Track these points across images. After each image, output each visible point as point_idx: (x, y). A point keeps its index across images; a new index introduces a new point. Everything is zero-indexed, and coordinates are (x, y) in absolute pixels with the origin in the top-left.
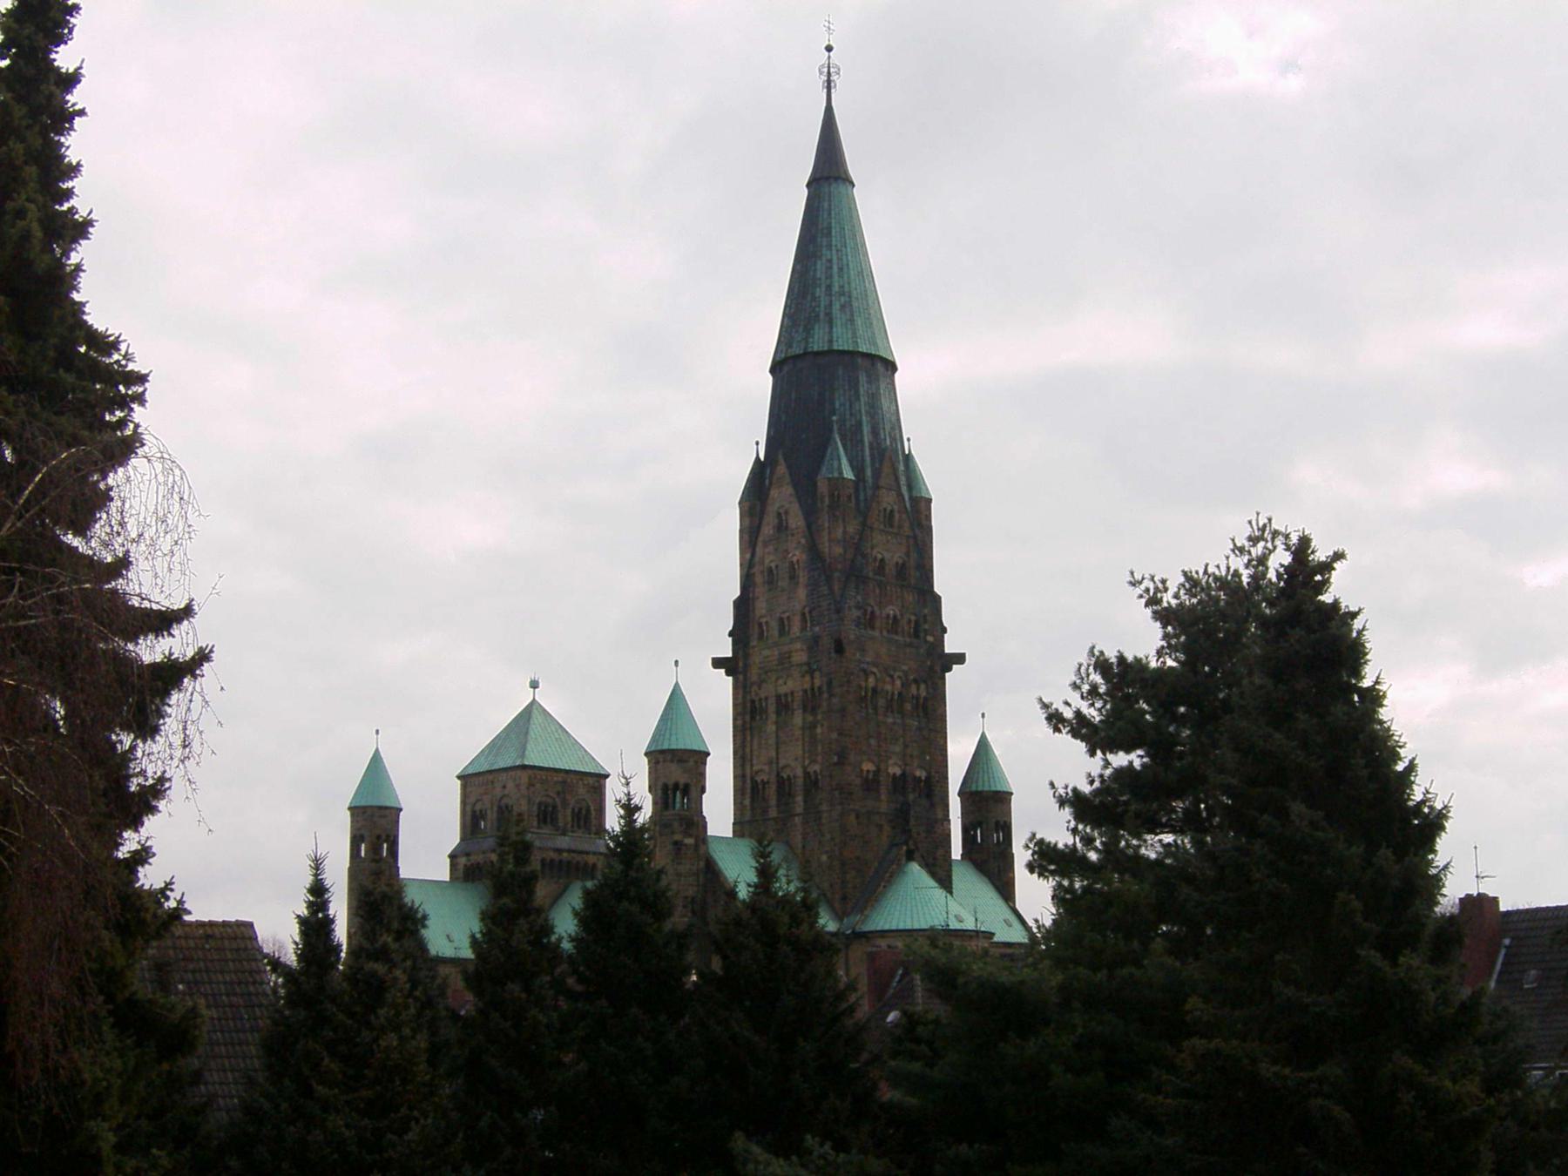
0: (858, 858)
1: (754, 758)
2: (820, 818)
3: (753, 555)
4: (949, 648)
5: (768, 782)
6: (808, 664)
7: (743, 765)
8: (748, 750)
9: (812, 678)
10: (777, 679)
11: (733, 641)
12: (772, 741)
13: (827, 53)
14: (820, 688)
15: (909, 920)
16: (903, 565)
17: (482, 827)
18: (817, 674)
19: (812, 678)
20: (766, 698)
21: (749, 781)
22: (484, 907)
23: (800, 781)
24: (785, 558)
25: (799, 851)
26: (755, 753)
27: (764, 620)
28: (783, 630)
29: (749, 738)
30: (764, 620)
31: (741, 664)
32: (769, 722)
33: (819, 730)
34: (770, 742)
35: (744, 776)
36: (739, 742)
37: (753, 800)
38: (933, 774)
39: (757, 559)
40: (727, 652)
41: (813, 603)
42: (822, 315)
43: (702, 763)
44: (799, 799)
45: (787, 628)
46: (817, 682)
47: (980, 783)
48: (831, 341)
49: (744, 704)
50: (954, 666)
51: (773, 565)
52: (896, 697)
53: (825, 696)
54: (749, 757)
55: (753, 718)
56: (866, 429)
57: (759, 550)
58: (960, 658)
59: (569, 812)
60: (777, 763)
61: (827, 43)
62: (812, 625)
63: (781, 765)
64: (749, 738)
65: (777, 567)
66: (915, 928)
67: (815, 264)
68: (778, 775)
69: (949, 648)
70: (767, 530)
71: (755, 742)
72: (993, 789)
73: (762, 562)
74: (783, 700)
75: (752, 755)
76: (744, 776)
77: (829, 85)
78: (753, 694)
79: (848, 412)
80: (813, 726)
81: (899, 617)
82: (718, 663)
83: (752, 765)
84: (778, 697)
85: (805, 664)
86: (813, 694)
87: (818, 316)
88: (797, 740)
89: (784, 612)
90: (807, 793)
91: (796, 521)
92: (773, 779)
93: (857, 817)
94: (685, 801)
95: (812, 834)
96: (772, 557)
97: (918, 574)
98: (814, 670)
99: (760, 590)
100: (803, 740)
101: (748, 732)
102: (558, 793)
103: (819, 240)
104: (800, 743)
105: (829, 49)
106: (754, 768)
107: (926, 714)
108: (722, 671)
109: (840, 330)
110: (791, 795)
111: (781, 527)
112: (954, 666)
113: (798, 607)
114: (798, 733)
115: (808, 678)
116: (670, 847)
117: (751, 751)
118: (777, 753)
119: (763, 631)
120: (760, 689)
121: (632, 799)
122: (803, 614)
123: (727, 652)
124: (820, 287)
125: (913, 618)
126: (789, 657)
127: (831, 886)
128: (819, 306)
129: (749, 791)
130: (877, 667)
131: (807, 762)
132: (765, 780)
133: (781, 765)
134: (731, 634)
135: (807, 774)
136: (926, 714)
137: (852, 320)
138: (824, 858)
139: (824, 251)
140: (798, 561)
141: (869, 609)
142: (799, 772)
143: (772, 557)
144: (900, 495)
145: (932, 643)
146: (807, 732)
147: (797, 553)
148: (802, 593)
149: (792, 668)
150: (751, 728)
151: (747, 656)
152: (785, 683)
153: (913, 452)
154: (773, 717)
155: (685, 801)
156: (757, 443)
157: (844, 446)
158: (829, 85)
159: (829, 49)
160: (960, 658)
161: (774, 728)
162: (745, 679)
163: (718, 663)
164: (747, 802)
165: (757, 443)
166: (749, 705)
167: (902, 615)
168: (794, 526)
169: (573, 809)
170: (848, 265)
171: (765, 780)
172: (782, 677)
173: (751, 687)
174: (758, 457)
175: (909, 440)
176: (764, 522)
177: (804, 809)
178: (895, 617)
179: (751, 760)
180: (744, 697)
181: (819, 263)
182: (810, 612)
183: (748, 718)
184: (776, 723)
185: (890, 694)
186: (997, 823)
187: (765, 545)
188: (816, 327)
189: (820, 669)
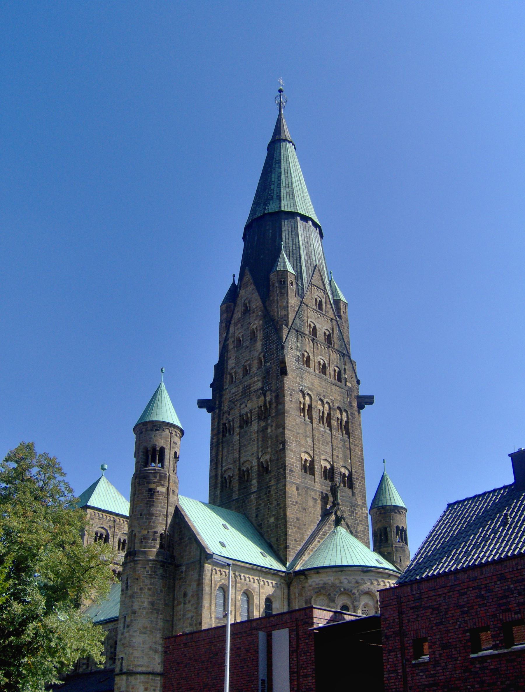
0: (298, 519)
1: (224, 461)
2: (269, 492)
3: (228, 333)
5: (232, 477)
6: (262, 388)
7: (216, 468)
8: (220, 458)
9: (265, 397)
10: (241, 405)
11: (213, 390)
12: (237, 447)
14: (270, 402)
15: (344, 559)
16: (329, 335)
18: (268, 393)
19: (265, 397)
20: (233, 420)
21: (219, 478)
23: (255, 469)
24: (248, 328)
25: (253, 520)
26: (225, 458)
27: (233, 371)
28: (246, 372)
29: (221, 449)
30: (233, 371)
31: (217, 402)
32: (235, 434)
33: (269, 430)
34: (235, 448)
35: (216, 475)
36: (214, 453)
37: (222, 491)
38: (354, 473)
39: (230, 335)
40: (208, 394)
41: (266, 349)
42: (275, 197)
44: (254, 482)
45: (248, 371)
46: (268, 399)
47: (385, 502)
48: (280, 207)
49: (218, 426)
51: (240, 335)
52: (326, 416)
53: (274, 406)
54: (220, 463)
55: (224, 436)
56: (303, 253)
57: (232, 329)
59: (117, 540)
60: (239, 460)
62: (265, 363)
63: (242, 461)
64: (221, 449)
65: (243, 335)
66: (343, 564)
67: (271, 176)
68: (239, 469)
70: (237, 315)
71: (225, 450)
72: (394, 504)
73: (233, 336)
74: (245, 417)
75: (222, 460)
76: (216, 475)
78: (224, 419)
79: (291, 243)
80: (265, 428)
81: (327, 365)
82: (202, 404)
83: (222, 467)
84: (241, 416)
85: (260, 389)
86: (266, 409)
87: (272, 197)
88: (254, 441)
89: (247, 361)
90: (260, 475)
91: (256, 303)
92: (236, 472)
93: (297, 489)
95: (263, 505)
96: (240, 331)
97: (339, 343)
98: (266, 391)
100: (258, 440)
101: (221, 445)
102: (110, 527)
103: (274, 166)
104: (255, 443)
106: (224, 469)
107: (348, 433)
108: (205, 410)
109: (286, 203)
110: (249, 480)
111: (247, 311)
113: (256, 354)
114: (255, 436)
115: (262, 398)
116: (146, 493)
117: (222, 458)
118: (240, 455)
119: (232, 378)
120: (229, 415)
122: (260, 359)
123: (208, 394)
124: (274, 185)
125: (337, 369)
126: (250, 388)
127: (277, 540)
128: (273, 193)
129: (219, 485)
130: (312, 391)
131: (260, 454)
132: (231, 475)
133: (242, 461)
134: (212, 386)
135: (260, 464)
136: (348, 433)
137: (294, 199)
138: (272, 520)
139: (277, 169)
140: (256, 328)
141: (306, 354)
142: (255, 463)
143: (240, 331)
144: (325, 293)
145: (350, 388)
146: (261, 434)
147: (256, 322)
148: (259, 345)
149: (251, 395)
150: (222, 443)
151: (221, 396)
152: (246, 406)
154: (237, 430)
156: (234, 276)
157: (289, 259)
161: (238, 437)
162: (220, 411)
163: (202, 404)
164: (218, 492)
165: (234, 276)
166: (221, 427)
167: (329, 364)
168: (254, 307)
169: (120, 540)
170: (302, 469)
171: (231, 475)
172: (244, 402)
173: (223, 416)
174: (234, 283)
176: (236, 311)
177: (258, 488)
178: (324, 365)
179: (222, 463)
180: (219, 423)
181: (273, 175)
182: (264, 356)
183: (221, 436)
184: (239, 434)
185: (321, 412)
186: (397, 527)
187: (236, 324)
188: (271, 202)
189: (270, 389)
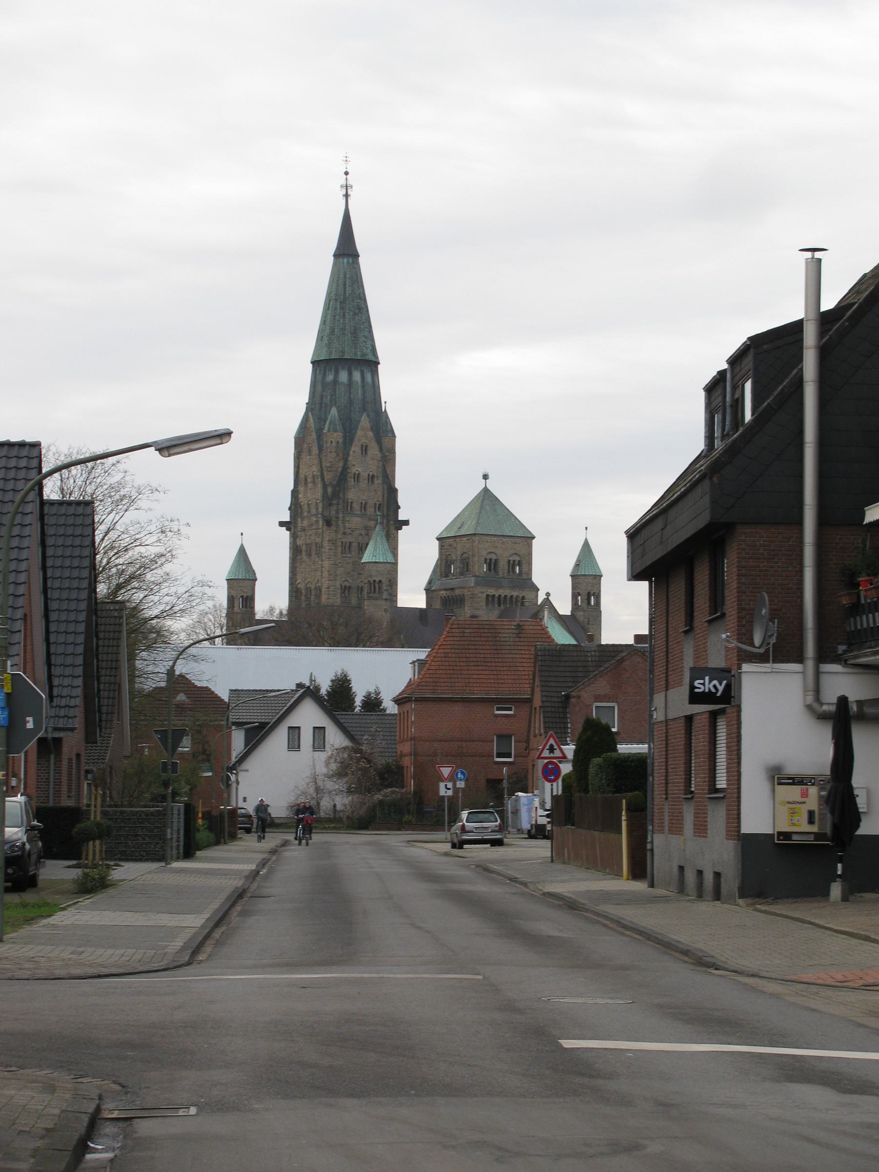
4: (402, 517)
13: (345, 176)
17: (517, 571)
40: (287, 518)
43: (392, 453)
50: (404, 527)
58: (406, 523)
61: (345, 170)
69: (402, 517)
77: (347, 196)
82: (282, 524)
94: (765, 347)
99: (301, 489)
105: (346, 173)
112: (404, 527)
121: (318, 689)
123: (287, 518)
153: (387, 410)
155: (765, 347)
158: (347, 196)
159: (346, 173)
160: (406, 523)
163: (282, 524)
175: (385, 402)
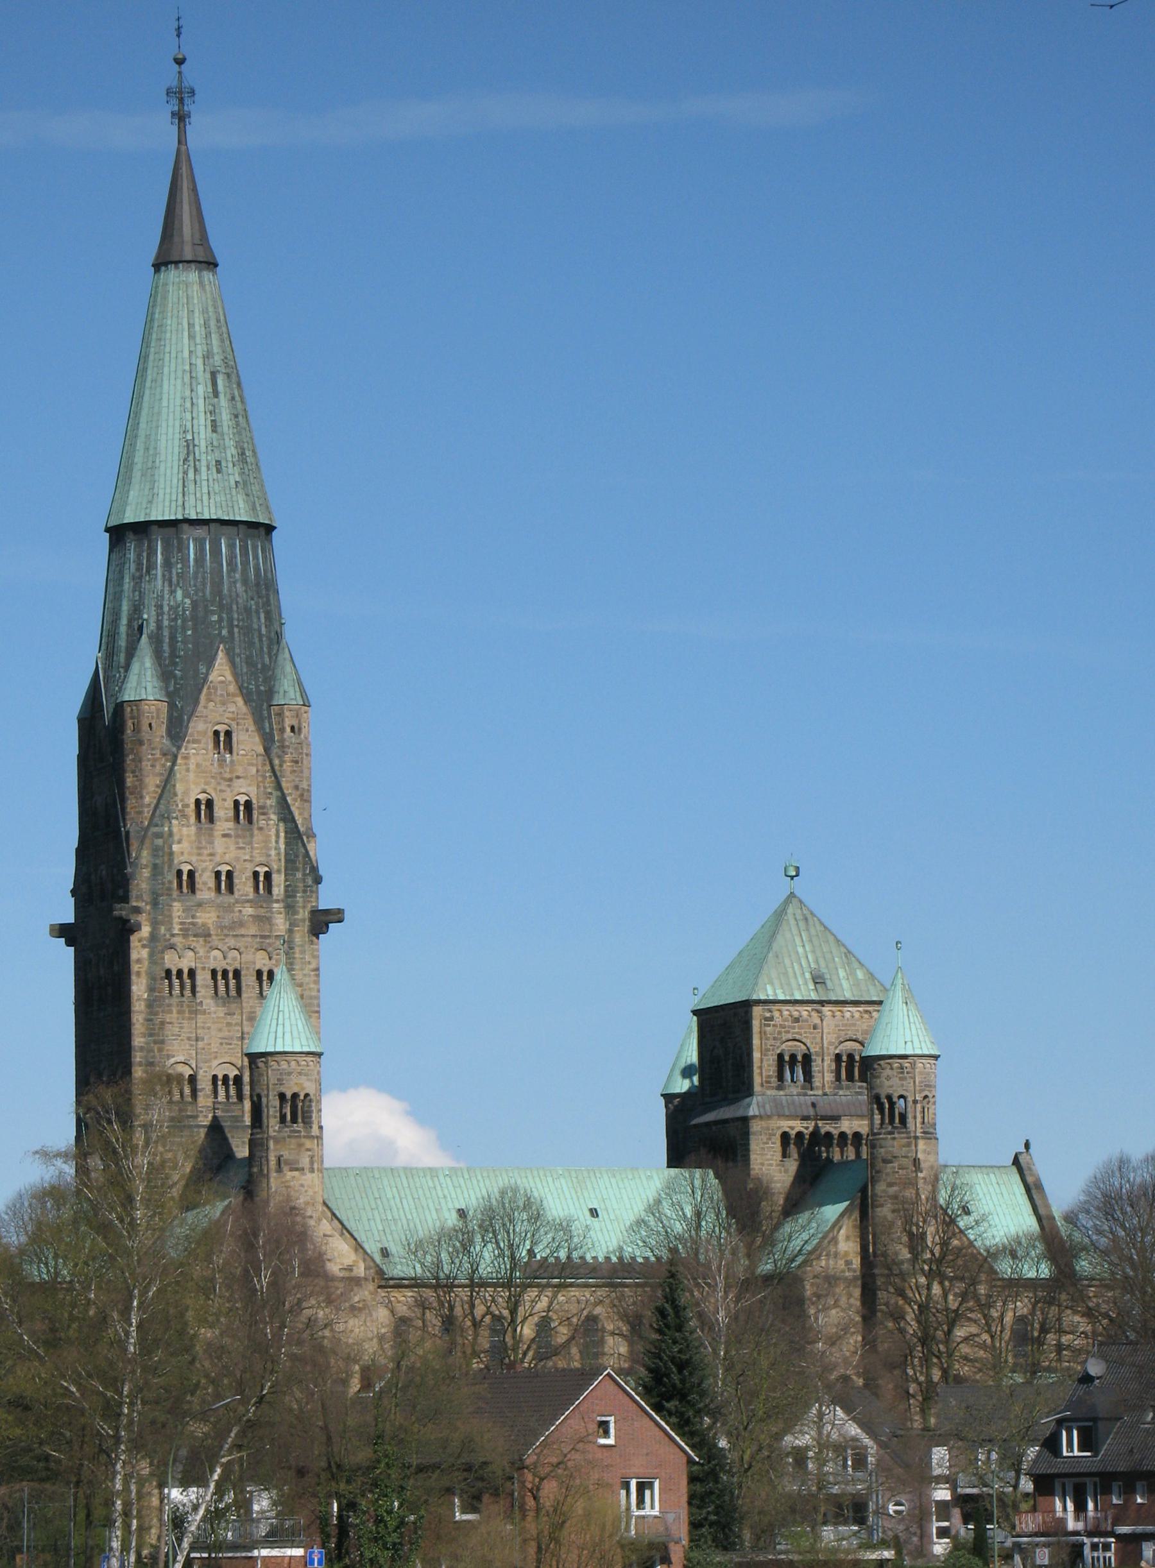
22: (638, 1252)
123: (69, 917)
